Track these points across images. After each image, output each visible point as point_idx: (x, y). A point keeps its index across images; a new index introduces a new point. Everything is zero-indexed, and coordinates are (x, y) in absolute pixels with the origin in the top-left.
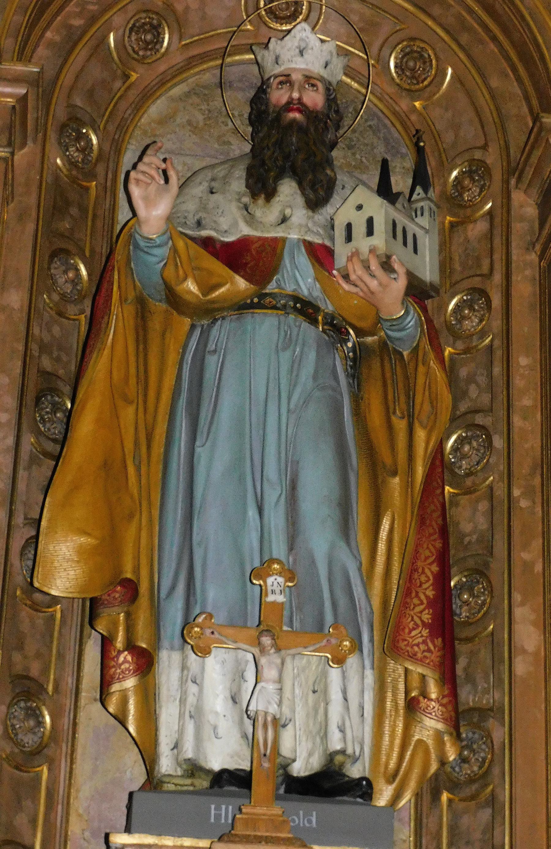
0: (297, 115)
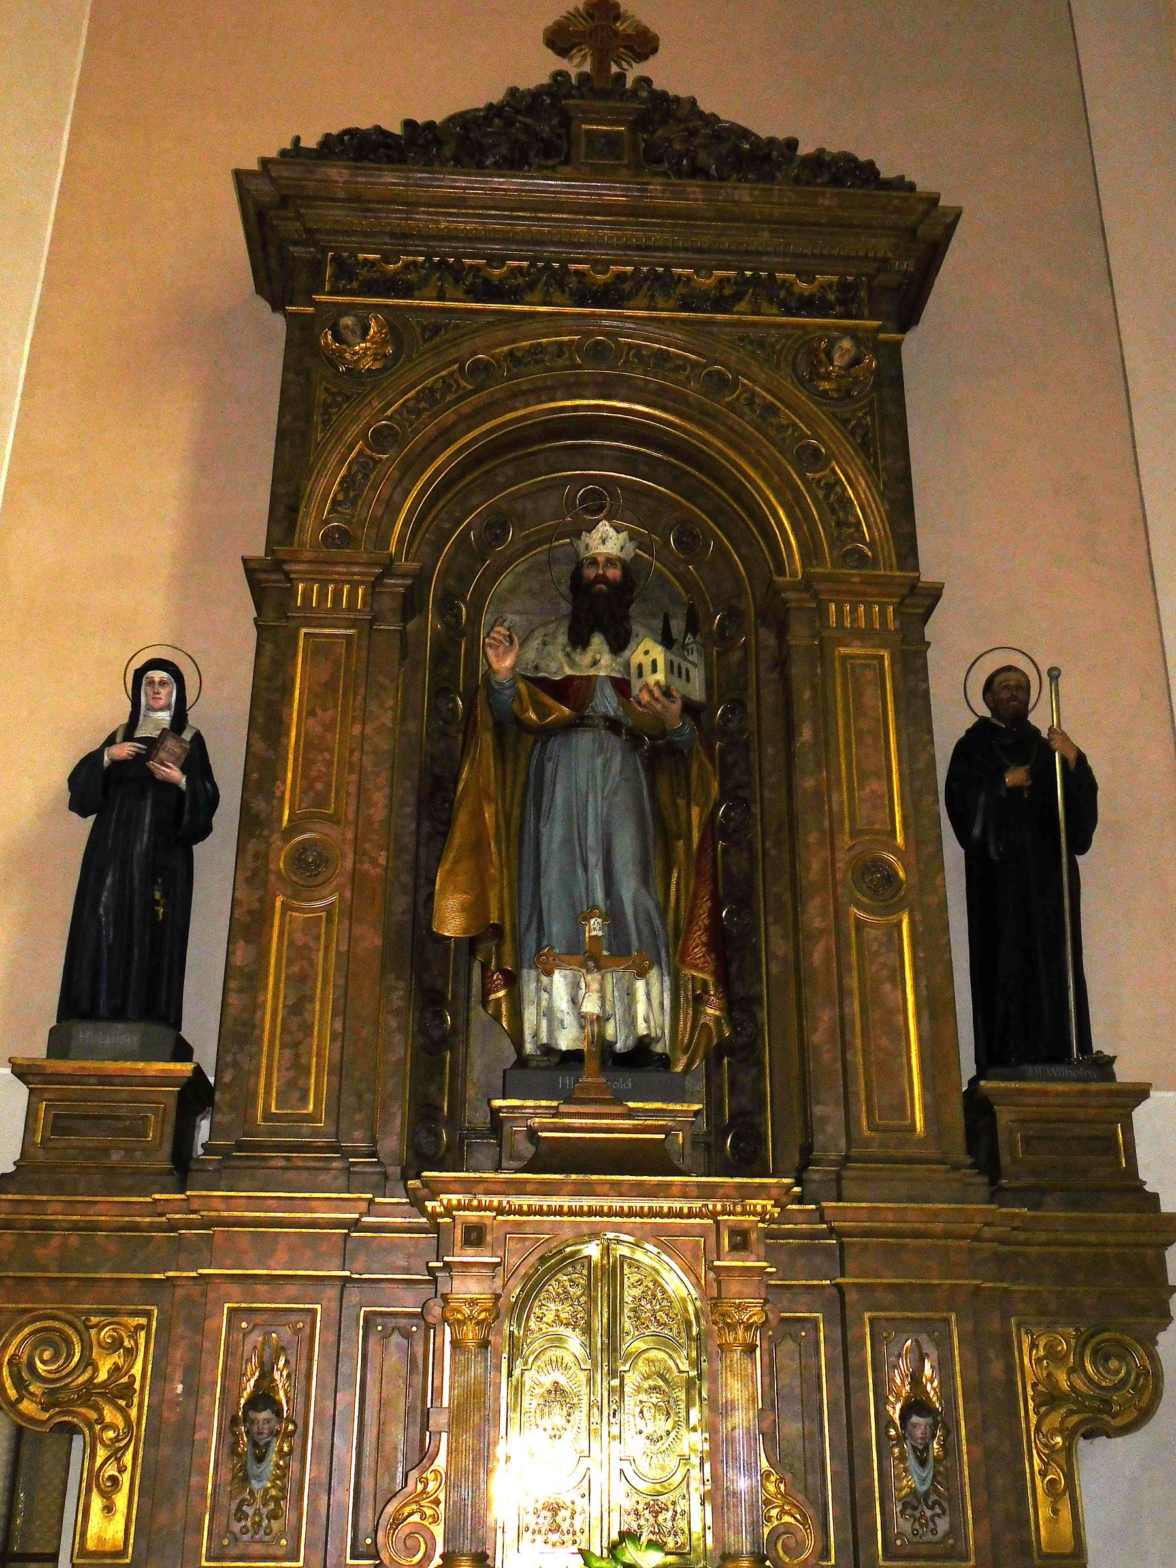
0: (604, 587)
